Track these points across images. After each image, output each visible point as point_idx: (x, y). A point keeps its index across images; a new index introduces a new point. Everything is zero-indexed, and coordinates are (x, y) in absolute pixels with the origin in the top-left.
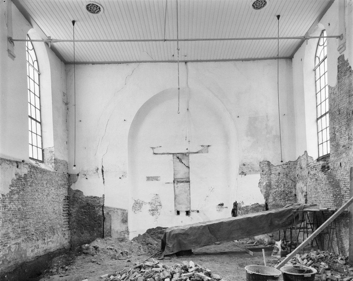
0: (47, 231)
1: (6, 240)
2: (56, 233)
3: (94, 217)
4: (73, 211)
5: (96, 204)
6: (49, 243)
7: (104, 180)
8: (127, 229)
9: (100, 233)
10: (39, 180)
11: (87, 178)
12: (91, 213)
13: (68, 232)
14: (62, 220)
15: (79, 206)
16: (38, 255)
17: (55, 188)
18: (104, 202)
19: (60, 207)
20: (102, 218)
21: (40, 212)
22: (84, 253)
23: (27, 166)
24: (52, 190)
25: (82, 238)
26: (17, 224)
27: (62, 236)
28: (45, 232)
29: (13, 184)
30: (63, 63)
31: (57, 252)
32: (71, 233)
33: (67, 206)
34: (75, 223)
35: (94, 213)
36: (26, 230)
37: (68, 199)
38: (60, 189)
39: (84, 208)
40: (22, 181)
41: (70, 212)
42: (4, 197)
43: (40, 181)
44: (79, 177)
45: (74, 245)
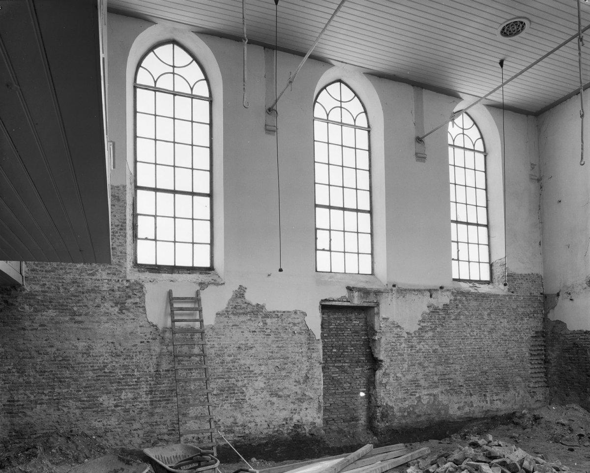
1: (414, 388)
4: (553, 355)
10: (473, 310)
12: (581, 361)
13: (543, 390)
16: (471, 415)
21: (476, 356)
22: (513, 422)
23: (449, 293)
24: (501, 322)
26: (432, 369)
29: (424, 319)
30: (531, 117)
34: (555, 377)
35: (587, 361)
36: (448, 379)
39: (569, 352)
40: (439, 315)
41: (549, 358)
42: (409, 336)
43: (474, 312)
44: (560, 298)
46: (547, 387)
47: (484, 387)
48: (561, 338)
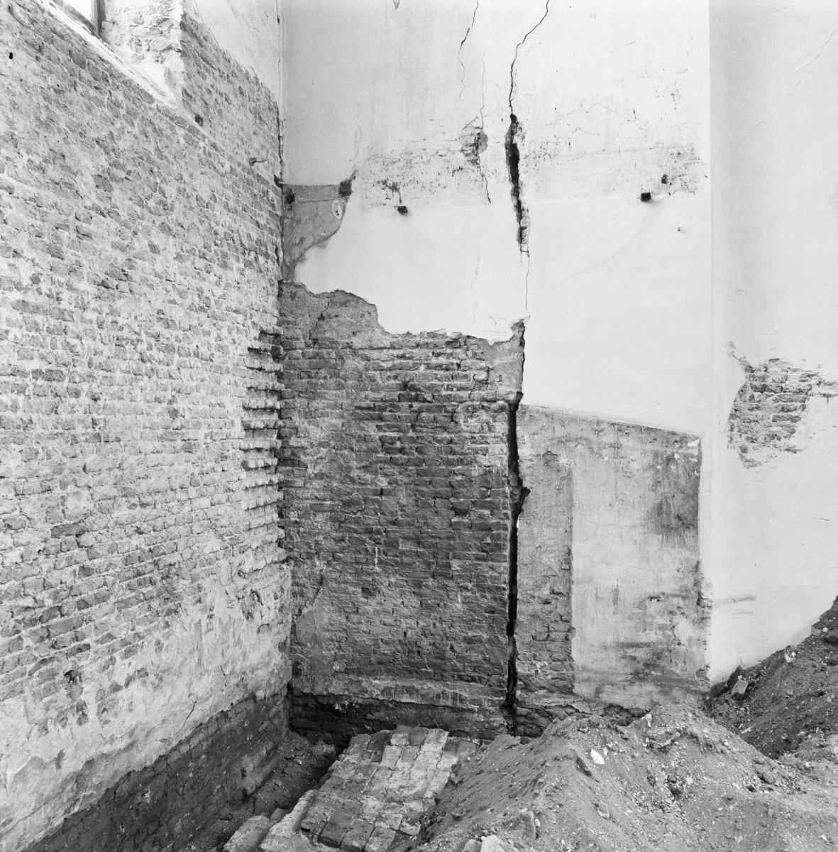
0: (101, 599)
2: (187, 601)
3: (451, 485)
5: (461, 389)
6: (123, 693)
7: (520, 217)
8: (689, 582)
9: (487, 601)
11: (403, 210)
13: (277, 577)
14: (240, 494)
15: (346, 402)
17: (187, 247)
18: (521, 379)
19: (223, 394)
20: (507, 490)
24: (154, 249)
25: (369, 622)
27: (238, 614)
28: (84, 604)
31: (195, 742)
32: (295, 584)
33: (270, 403)
35: (453, 452)
37: (276, 357)
38: (224, 266)
39: (381, 418)
41: (293, 442)
44: (354, 201)
45: (312, 667)
46: (286, 561)
47: (69, 626)
48: (348, 361)
